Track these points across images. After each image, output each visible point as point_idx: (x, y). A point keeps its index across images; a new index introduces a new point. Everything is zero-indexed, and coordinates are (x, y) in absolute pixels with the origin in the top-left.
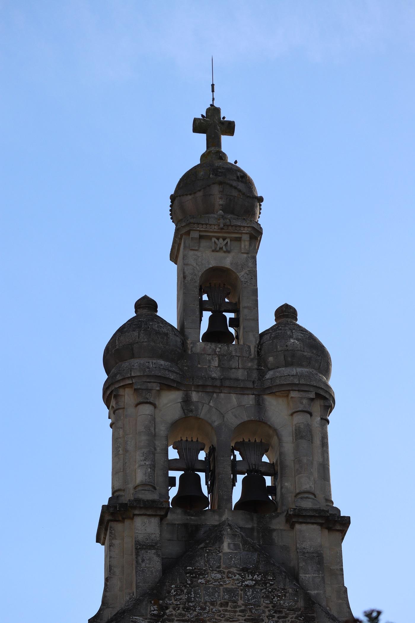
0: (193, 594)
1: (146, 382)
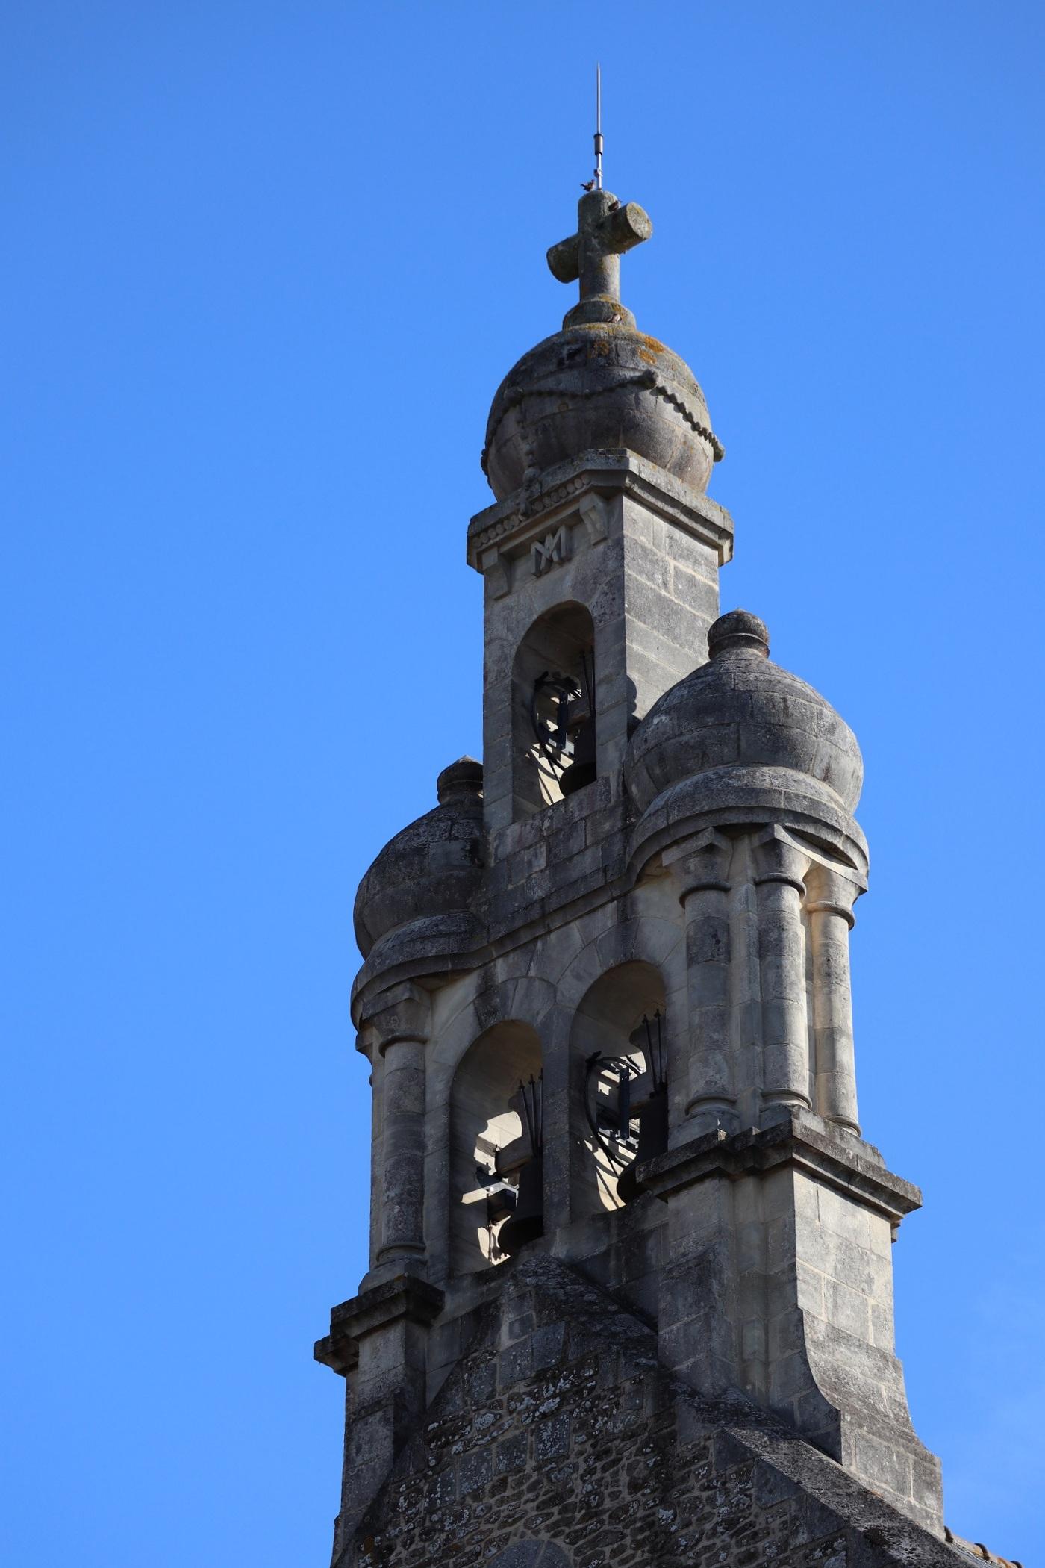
0: (439, 1490)
1: (382, 992)
